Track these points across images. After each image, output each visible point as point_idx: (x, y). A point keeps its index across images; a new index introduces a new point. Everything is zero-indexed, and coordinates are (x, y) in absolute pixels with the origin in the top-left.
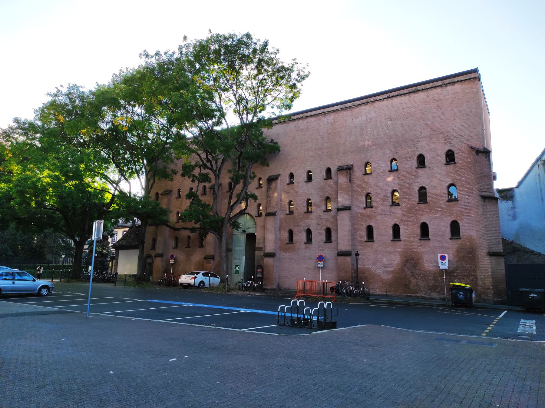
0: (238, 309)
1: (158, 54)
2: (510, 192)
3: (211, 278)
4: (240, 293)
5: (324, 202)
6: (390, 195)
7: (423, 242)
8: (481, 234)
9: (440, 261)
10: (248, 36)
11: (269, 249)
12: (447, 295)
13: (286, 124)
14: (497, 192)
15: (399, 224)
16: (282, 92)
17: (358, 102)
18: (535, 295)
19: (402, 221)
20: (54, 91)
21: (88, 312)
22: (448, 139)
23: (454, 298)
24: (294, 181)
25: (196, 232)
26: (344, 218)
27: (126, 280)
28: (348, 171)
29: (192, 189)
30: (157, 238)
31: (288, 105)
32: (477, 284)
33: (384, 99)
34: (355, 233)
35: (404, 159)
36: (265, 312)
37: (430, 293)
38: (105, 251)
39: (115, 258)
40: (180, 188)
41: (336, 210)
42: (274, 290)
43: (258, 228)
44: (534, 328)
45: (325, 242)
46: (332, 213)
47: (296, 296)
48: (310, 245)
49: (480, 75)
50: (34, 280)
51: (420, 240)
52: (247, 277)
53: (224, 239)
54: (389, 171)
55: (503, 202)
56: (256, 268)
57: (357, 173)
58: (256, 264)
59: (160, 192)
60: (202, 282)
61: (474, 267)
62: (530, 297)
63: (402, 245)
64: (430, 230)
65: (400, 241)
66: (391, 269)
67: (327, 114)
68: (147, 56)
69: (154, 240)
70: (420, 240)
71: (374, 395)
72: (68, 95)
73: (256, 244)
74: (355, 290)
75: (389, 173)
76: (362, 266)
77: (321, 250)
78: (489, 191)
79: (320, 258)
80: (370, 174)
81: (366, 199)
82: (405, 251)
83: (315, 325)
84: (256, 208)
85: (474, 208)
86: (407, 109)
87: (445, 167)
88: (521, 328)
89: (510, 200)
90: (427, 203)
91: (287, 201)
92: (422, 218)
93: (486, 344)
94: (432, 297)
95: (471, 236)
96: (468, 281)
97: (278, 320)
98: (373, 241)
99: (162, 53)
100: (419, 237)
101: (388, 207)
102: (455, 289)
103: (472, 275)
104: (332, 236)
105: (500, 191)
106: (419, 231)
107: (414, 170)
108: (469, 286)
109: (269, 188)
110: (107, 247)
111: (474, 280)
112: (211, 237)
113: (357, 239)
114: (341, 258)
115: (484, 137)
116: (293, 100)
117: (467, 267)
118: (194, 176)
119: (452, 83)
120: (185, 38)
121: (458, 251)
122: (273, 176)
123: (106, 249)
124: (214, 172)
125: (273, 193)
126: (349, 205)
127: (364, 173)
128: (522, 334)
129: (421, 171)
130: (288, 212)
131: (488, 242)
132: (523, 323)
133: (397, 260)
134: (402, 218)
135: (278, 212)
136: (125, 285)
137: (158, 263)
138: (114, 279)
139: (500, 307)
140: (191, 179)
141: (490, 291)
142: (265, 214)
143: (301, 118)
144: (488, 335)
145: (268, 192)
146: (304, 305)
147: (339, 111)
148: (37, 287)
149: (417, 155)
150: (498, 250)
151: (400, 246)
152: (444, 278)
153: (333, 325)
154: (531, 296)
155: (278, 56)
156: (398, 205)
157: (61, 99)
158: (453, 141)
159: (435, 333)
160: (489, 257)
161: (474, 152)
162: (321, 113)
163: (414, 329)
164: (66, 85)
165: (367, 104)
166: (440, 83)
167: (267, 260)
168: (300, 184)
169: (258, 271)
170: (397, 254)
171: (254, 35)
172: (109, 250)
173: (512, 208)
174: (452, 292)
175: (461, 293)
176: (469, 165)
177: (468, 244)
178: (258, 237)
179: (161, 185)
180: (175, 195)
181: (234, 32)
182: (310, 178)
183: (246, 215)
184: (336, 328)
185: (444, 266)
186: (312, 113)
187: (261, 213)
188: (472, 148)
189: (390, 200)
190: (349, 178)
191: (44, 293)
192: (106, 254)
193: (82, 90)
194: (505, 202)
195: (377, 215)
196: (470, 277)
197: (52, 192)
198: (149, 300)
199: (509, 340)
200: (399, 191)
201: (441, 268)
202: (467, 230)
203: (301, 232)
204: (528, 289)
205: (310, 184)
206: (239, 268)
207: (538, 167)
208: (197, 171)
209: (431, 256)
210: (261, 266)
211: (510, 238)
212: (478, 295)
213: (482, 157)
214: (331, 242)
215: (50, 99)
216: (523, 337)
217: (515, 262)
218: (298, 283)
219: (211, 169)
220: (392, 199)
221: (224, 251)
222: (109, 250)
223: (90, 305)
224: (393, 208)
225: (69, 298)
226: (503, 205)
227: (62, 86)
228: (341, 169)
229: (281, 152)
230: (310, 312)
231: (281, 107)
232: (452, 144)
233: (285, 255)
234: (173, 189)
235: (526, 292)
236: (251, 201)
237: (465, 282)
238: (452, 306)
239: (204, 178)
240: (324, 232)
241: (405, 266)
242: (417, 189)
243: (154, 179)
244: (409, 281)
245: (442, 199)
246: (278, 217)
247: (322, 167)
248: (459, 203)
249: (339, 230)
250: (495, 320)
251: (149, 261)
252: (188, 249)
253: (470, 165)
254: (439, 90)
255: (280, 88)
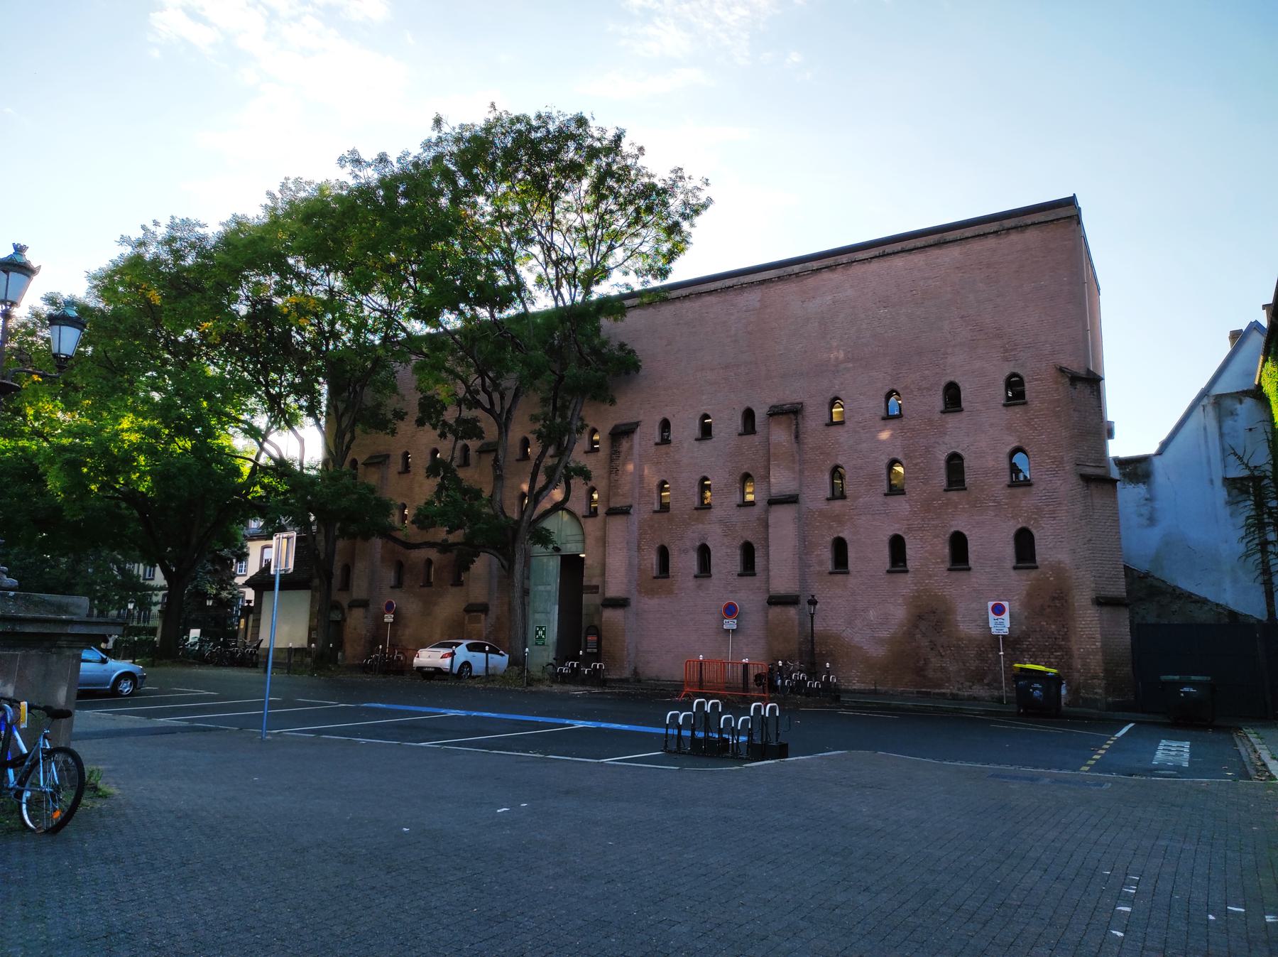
0: (568, 722)
1: (383, 159)
2: (1143, 466)
3: (489, 655)
4: (556, 688)
5: (738, 485)
6: (885, 471)
7: (954, 574)
8: (1079, 559)
9: (992, 616)
10: (581, 121)
11: (613, 591)
12: (1005, 690)
13: (654, 308)
14: (1116, 464)
15: (904, 536)
16: (648, 240)
17: (815, 265)
18: (1192, 690)
19: (910, 529)
20: (138, 234)
21: (264, 729)
22: (1012, 350)
23: (1023, 697)
24: (672, 437)
25: (451, 552)
26: (783, 522)
27: (291, 660)
28: (793, 416)
29: (435, 451)
30: (354, 564)
31: (660, 269)
32: (1070, 667)
33: (871, 258)
34: (806, 554)
35: (915, 393)
36: (625, 727)
37: (970, 687)
38: (224, 594)
39: (253, 612)
40: (409, 451)
41: (765, 503)
42: (626, 681)
43: (588, 541)
44: (1187, 756)
45: (739, 575)
46: (756, 511)
47: (684, 693)
48: (705, 581)
49: (1080, 209)
50: (104, 661)
51: (949, 570)
52: (562, 656)
53: (518, 567)
54: (884, 419)
55: (1128, 486)
56: (584, 631)
57: (813, 421)
58: (585, 623)
59: (361, 459)
60: (466, 664)
61: (1066, 630)
62: (1182, 695)
63: (909, 582)
64: (972, 547)
65: (907, 571)
66: (885, 634)
67: (746, 287)
68: (357, 162)
69: (347, 570)
70: (949, 570)
71: (894, 860)
72: (170, 241)
73: (584, 579)
74: (808, 680)
75: (883, 422)
76: (822, 629)
77: (731, 592)
78: (1097, 464)
79: (730, 611)
80: (841, 423)
81: (833, 478)
82: (916, 594)
83: (743, 749)
84: (585, 497)
85: (1065, 502)
86: (922, 283)
87: (1004, 410)
88: (1159, 755)
89: (1144, 483)
90: (966, 489)
91: (655, 482)
92: (953, 522)
93: (1089, 785)
94: (976, 696)
95: (1060, 562)
96: (1052, 660)
97: (666, 741)
98: (847, 573)
99: (393, 158)
100: (948, 565)
101: (881, 499)
102: (1024, 678)
103: (1061, 648)
104: (756, 560)
105: (1122, 463)
106: (947, 551)
107: (937, 416)
108: (1055, 671)
109: (614, 454)
110: (231, 585)
111: (1065, 657)
112: (483, 564)
113: (812, 569)
114: (776, 611)
115: (1087, 346)
116: (673, 258)
117: (1050, 630)
118: (445, 423)
119: (1021, 227)
120: (438, 122)
121: (1030, 595)
122: (624, 425)
123: (227, 589)
124: (497, 418)
125: (624, 464)
126: (793, 493)
127: (827, 421)
128: (1162, 767)
129: (952, 420)
130: (656, 507)
131: (1095, 577)
132: (1165, 748)
133: (899, 613)
134: (911, 522)
135: (636, 506)
136: (288, 673)
137: (357, 622)
138: (253, 659)
139: (1119, 715)
140: (438, 431)
141: (1100, 681)
142: (605, 511)
143: (686, 296)
144: (1093, 769)
145: (612, 460)
146: (720, 710)
147: (773, 282)
148: (111, 676)
149: (943, 383)
150: (1115, 593)
151: (906, 584)
152: (1002, 653)
153: (782, 752)
154: (1184, 692)
155: (641, 162)
156: (901, 492)
157: (150, 252)
158: (1022, 353)
159: (987, 766)
160: (1097, 608)
161: (1067, 380)
162: (732, 287)
163: (945, 760)
164: (165, 221)
165: (835, 270)
166: (994, 226)
167: (609, 614)
168: (686, 445)
169: (589, 638)
170: (900, 601)
171: (594, 119)
172: (236, 592)
173: (1146, 500)
174: (1017, 684)
175: (1037, 685)
176: (1055, 408)
177: (1051, 579)
178: (588, 562)
179: (366, 444)
180: (396, 465)
181: (548, 110)
182: (706, 431)
183: (560, 512)
184: (787, 757)
185: (1000, 627)
186: (712, 286)
187: (596, 509)
188: (1062, 370)
189: (885, 483)
190: (793, 431)
191: (126, 690)
192: (228, 600)
193: (201, 231)
194: (1133, 485)
195: (855, 515)
196: (1056, 652)
197: (143, 463)
198: (365, 705)
199: (1134, 777)
200: (904, 462)
201: (994, 631)
202: (1050, 548)
203: (685, 551)
204: (1177, 677)
205: (707, 445)
206: (544, 634)
207: (1204, 410)
208: (450, 415)
209: (974, 605)
210: (595, 627)
211: (1142, 565)
212: (1074, 692)
213: (1083, 390)
214: (754, 575)
215: (128, 251)
216: (1163, 772)
217: (1151, 619)
218: (686, 664)
219: (490, 411)
220: (890, 480)
221: (517, 594)
222: (236, 592)
223: (268, 713)
224: (891, 499)
225: (168, 701)
226: (1129, 494)
227: (156, 223)
228: (776, 412)
229: (642, 373)
230: (733, 725)
231: (645, 272)
232: (1020, 362)
233: (651, 603)
234: (391, 453)
235: (1173, 683)
236: (577, 483)
237: (1046, 662)
238: (1019, 714)
239: (469, 429)
240: (738, 552)
241: (917, 627)
242: (942, 457)
243: (353, 432)
244: (925, 659)
245: (996, 480)
246: (635, 518)
247: (734, 406)
248: (1033, 489)
249: (772, 549)
250: (1109, 742)
251: (336, 616)
252: (426, 589)
253: (1058, 407)
254: (991, 242)
255: (643, 232)
